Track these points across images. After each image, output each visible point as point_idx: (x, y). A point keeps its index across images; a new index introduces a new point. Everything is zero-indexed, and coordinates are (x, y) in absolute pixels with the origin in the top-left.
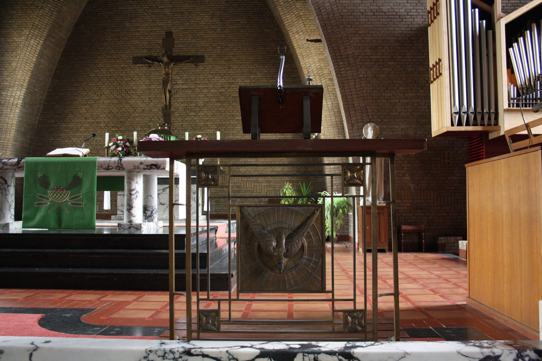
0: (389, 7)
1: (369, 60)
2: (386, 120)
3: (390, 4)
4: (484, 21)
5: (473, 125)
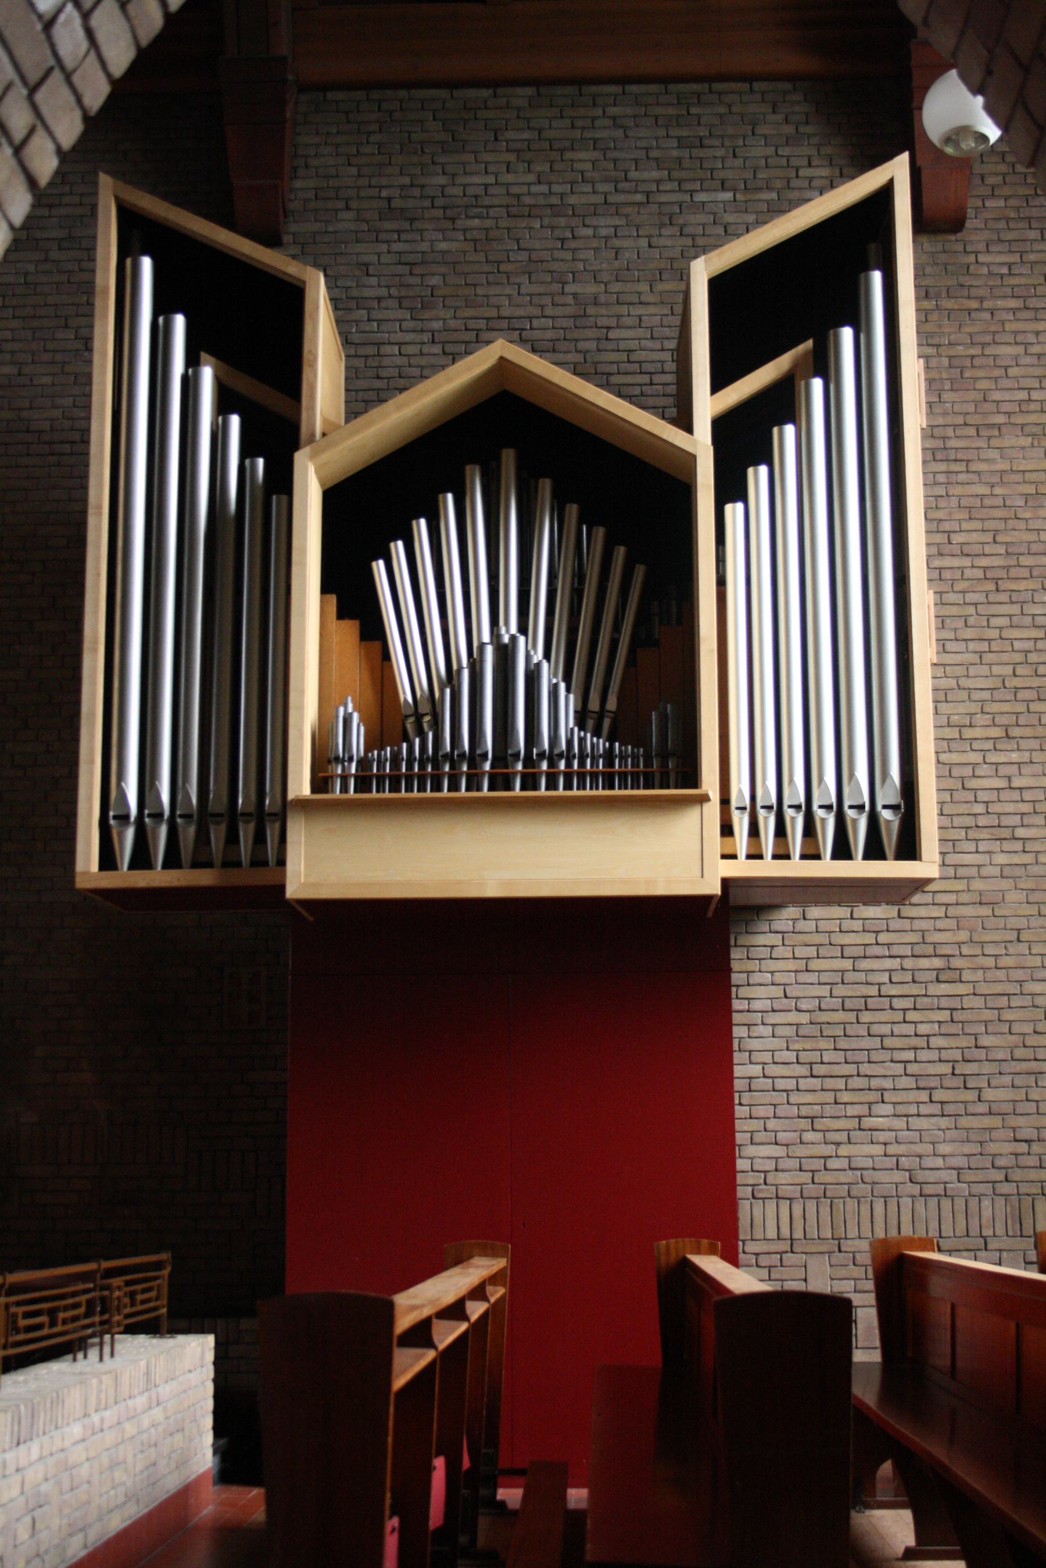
0: (57, 413)
3: (59, 401)
4: (261, 462)
5: (195, 865)
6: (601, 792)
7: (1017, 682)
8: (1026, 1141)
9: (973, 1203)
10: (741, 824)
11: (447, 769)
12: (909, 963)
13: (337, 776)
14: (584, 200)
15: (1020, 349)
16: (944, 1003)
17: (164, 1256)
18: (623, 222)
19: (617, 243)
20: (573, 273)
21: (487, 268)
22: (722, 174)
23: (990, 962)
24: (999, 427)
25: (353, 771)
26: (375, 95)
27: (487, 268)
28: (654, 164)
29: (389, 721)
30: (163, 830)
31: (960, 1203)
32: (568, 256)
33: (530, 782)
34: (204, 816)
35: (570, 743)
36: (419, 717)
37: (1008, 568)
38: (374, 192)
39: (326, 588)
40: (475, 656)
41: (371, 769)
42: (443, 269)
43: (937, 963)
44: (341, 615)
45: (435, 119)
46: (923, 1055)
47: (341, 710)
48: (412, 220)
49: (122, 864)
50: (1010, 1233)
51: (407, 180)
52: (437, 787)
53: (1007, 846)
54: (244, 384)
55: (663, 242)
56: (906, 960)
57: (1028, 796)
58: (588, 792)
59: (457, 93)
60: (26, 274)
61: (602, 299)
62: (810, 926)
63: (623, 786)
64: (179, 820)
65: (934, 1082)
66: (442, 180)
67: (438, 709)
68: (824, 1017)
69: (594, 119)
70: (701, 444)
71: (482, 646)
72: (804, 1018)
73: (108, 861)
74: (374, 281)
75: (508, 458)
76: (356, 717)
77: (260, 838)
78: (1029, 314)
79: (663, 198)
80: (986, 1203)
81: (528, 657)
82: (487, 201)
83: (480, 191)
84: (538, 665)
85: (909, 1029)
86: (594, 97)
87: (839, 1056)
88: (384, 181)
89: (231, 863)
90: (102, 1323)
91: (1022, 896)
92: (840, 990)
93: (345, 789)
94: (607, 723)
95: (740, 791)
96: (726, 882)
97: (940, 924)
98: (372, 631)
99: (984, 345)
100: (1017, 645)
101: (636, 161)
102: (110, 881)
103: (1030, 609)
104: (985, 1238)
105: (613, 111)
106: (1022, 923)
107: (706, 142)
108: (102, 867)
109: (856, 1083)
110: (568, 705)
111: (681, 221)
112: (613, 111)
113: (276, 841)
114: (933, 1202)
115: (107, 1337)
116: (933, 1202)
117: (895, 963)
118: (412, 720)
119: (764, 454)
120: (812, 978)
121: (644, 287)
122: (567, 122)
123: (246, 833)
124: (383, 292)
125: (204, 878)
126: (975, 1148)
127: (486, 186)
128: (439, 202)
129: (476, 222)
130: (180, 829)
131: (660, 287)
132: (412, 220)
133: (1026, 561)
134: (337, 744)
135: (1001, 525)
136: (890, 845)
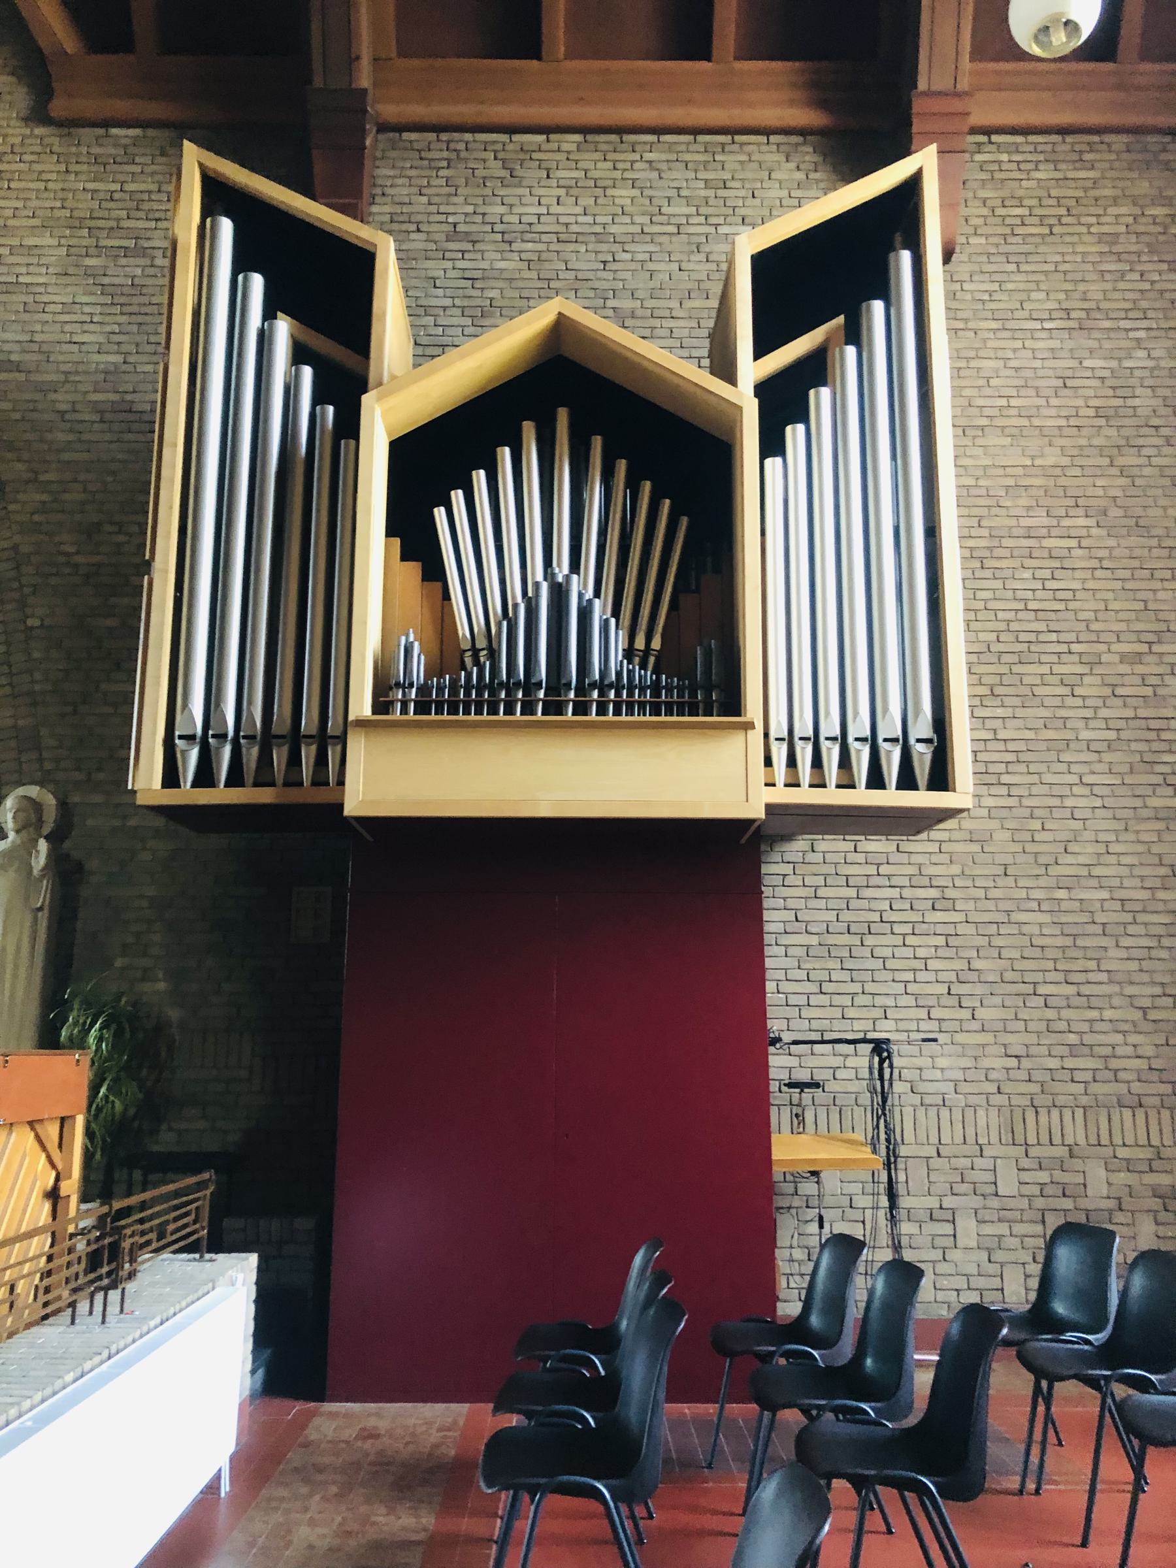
1: (67, 570)
2: (101, 776)
4: (331, 409)
5: (256, 784)
6: (648, 718)
7: (1001, 647)
8: (1016, 1057)
9: (969, 1113)
10: (780, 754)
11: (503, 695)
12: (907, 893)
13: (398, 700)
14: (624, 229)
15: (1001, 363)
16: (940, 929)
17: (206, 1176)
18: (657, 249)
19: (651, 266)
20: (614, 291)
21: (540, 284)
22: (743, 212)
23: (980, 893)
24: (982, 428)
25: (413, 696)
26: (444, 136)
27: (540, 284)
28: (684, 201)
29: (447, 653)
30: (227, 751)
31: (957, 1115)
32: (610, 276)
33: (581, 708)
34: (267, 739)
35: (619, 674)
36: (475, 652)
37: (990, 549)
38: (442, 218)
39: (390, 532)
40: (530, 595)
41: (431, 695)
42: (501, 284)
43: (933, 893)
44: (404, 557)
45: (496, 158)
46: (921, 976)
47: (403, 639)
48: (474, 242)
49: (185, 782)
50: (1003, 1141)
51: (470, 209)
52: (493, 711)
53: (994, 790)
54: (319, 343)
55: (691, 266)
56: (905, 890)
57: (1011, 746)
58: (635, 718)
59: (516, 137)
60: (133, 277)
61: (639, 312)
62: (818, 857)
63: (669, 713)
64: (242, 741)
65: (932, 1001)
66: (502, 209)
67: (495, 645)
68: (831, 939)
69: (633, 162)
70: (743, 397)
71: (537, 585)
72: (814, 940)
73: (171, 778)
74: (440, 292)
75: (563, 417)
76: (416, 645)
77: (321, 760)
78: (1007, 334)
79: (691, 230)
80: (981, 1113)
81: (580, 595)
82: (539, 228)
83: (534, 219)
84: (590, 601)
85: (908, 952)
86: (633, 145)
87: (845, 976)
88: (451, 209)
89: (293, 782)
90: (109, 1274)
91: (1007, 835)
92: (846, 916)
93: (404, 711)
94: (652, 660)
95: (779, 722)
96: (769, 808)
97: (935, 859)
98: (434, 572)
99: (968, 359)
100: (1001, 615)
101: (669, 199)
102: (172, 797)
103: (1011, 584)
104: (980, 1146)
105: (648, 156)
106: (1009, 859)
107: (729, 184)
108: (164, 786)
109: (860, 1000)
110: (618, 642)
111: (707, 250)
112: (648, 156)
113: (337, 768)
114: (932, 1112)
115: (114, 1295)
116: (932, 1112)
117: (895, 893)
118: (470, 653)
119: (802, 415)
120: (821, 904)
121: (674, 304)
122: (609, 165)
123: (307, 754)
124: (448, 302)
125: (265, 796)
126: (969, 1063)
127: (539, 215)
128: (498, 228)
129: (530, 246)
130: (244, 750)
131: (688, 304)
132: (474, 242)
133: (1007, 542)
134: (398, 670)
135: (984, 512)
136: (922, 776)
